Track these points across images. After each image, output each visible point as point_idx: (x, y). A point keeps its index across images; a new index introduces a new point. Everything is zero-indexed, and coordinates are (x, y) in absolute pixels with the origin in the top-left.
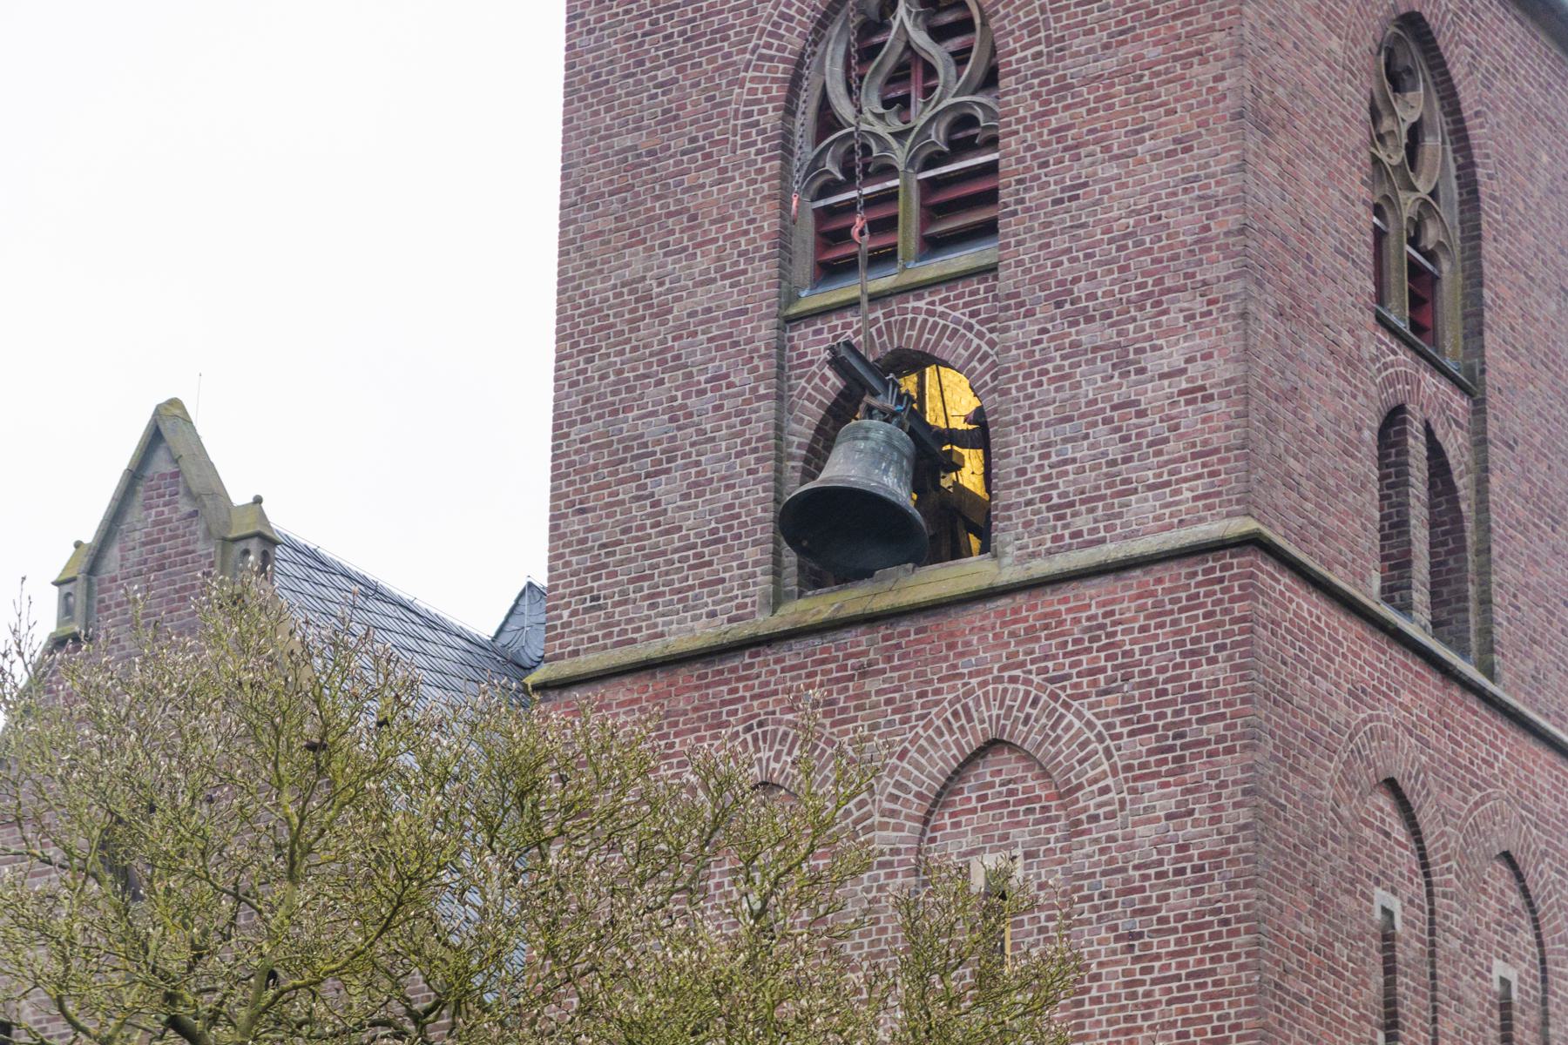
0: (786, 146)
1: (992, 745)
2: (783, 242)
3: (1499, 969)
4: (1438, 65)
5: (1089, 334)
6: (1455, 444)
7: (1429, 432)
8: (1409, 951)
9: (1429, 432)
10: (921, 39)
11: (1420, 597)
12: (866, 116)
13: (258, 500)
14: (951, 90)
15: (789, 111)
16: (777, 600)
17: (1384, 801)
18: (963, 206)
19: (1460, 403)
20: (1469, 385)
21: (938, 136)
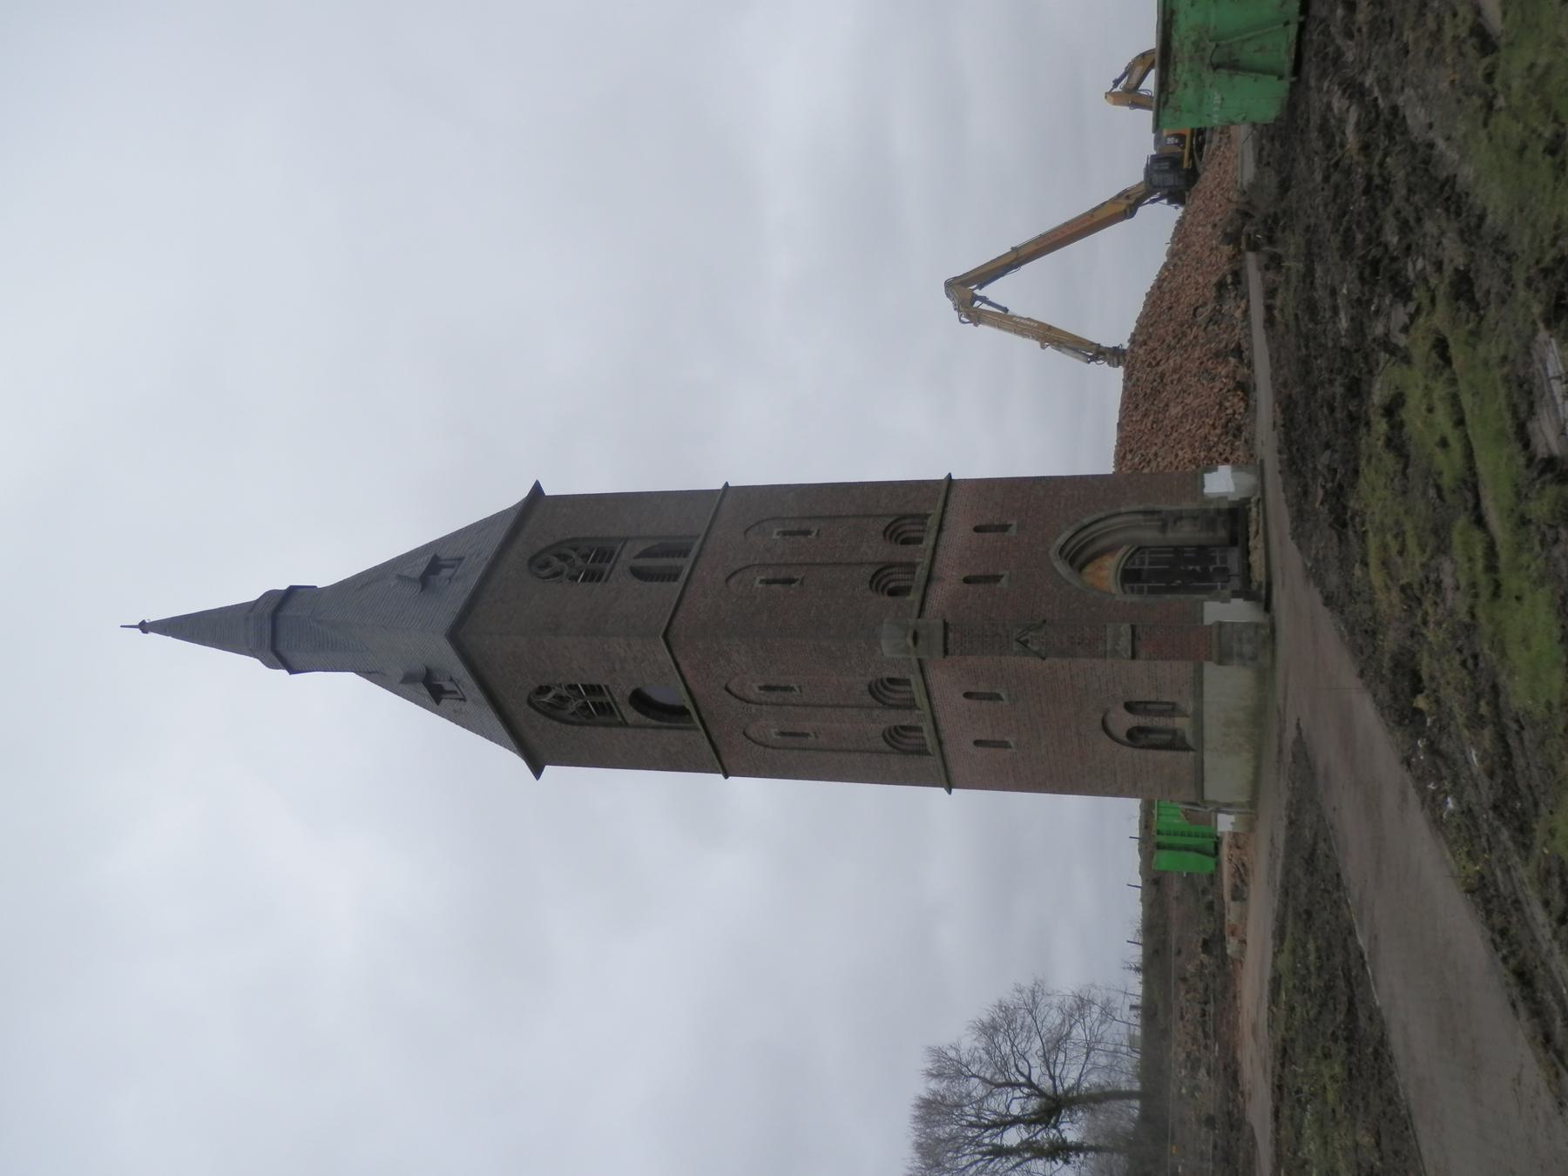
0: (581, 724)
1: (727, 689)
2: (606, 725)
3: (774, 536)
4: (542, 552)
5: (618, 666)
6: (641, 547)
7: (638, 556)
8: (770, 574)
9: (638, 556)
10: (551, 695)
11: (678, 561)
12: (573, 706)
13: (537, 771)
14: (564, 693)
15: (572, 723)
16: (696, 729)
17: (732, 581)
18: (593, 689)
19: (629, 545)
20: (626, 540)
21: (575, 692)
